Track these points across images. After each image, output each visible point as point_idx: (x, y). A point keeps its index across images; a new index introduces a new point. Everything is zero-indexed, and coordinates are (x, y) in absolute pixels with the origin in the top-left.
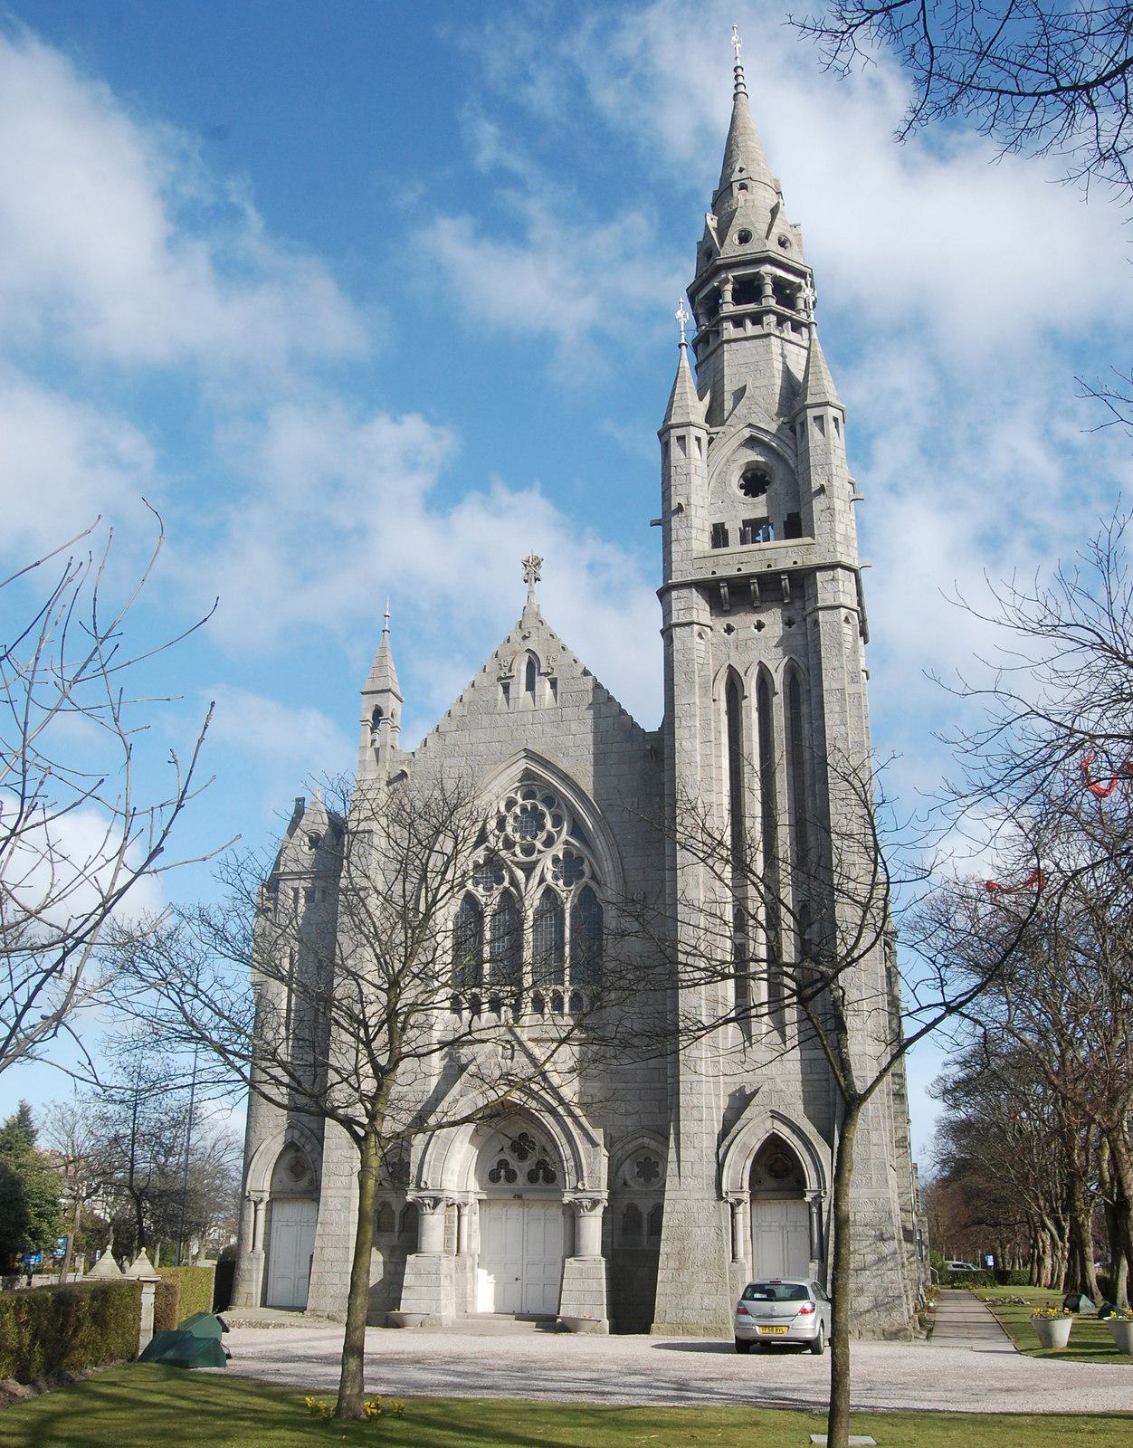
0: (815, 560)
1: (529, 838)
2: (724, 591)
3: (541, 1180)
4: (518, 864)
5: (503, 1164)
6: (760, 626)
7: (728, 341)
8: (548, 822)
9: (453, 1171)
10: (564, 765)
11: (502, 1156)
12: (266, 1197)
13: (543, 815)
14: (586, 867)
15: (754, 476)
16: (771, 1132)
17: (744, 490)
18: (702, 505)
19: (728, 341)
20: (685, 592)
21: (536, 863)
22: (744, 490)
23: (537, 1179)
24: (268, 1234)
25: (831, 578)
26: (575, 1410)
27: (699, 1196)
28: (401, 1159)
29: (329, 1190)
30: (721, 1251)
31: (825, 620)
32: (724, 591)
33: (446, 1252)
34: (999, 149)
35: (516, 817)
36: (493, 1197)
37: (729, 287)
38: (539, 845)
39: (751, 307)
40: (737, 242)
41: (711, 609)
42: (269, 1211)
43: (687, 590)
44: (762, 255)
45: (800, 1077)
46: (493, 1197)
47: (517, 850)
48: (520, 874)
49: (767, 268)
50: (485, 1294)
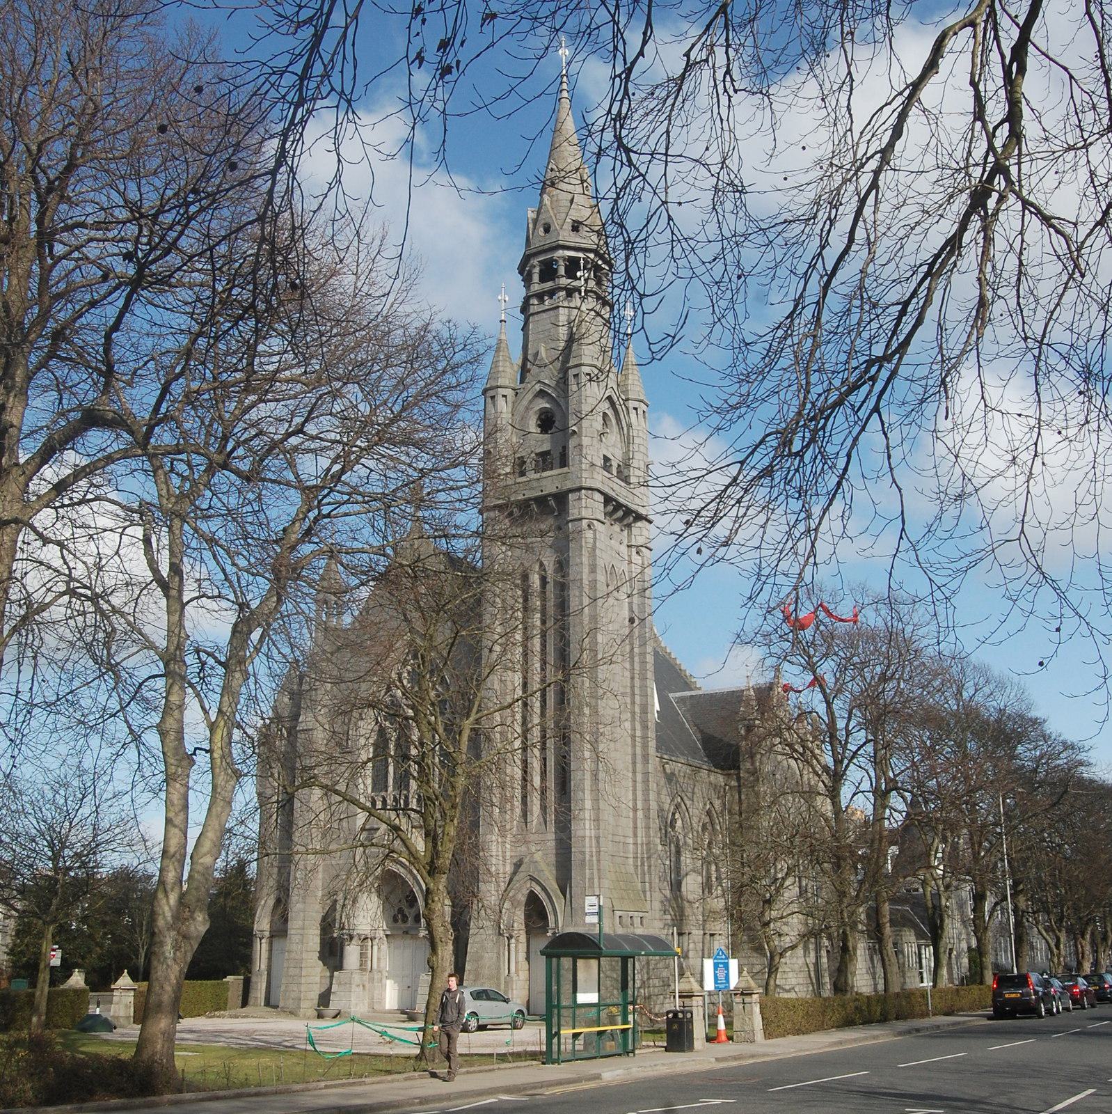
0: (569, 485)
5: (400, 911)
7: (533, 314)
12: (267, 934)
15: (547, 416)
19: (533, 314)
24: (270, 959)
26: (1018, 1033)
28: (1028, 779)
33: (361, 970)
34: (885, 63)
36: (395, 933)
37: (537, 270)
39: (549, 284)
40: (543, 234)
42: (271, 944)
44: (553, 245)
45: (554, 851)
46: (395, 933)
49: (561, 253)
50: (391, 996)
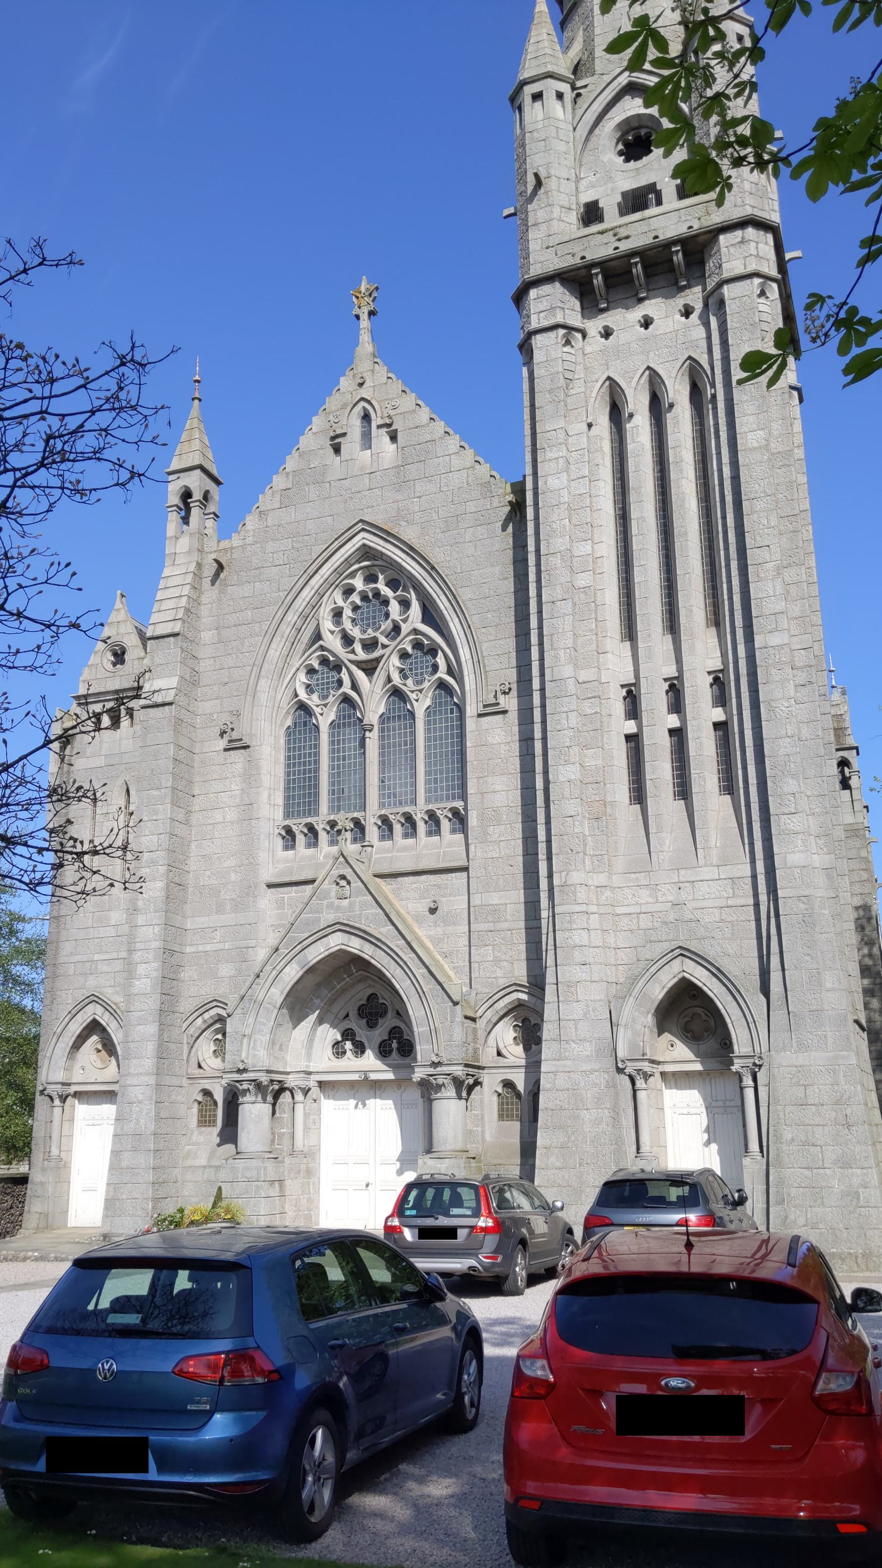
1: (370, 631)
2: (598, 281)
3: (349, 1053)
4: (359, 664)
6: (647, 323)
8: (394, 608)
9: (281, 1045)
10: (409, 534)
11: (347, 1025)
13: (386, 602)
14: (440, 660)
16: (680, 976)
17: (623, 157)
18: (566, 176)
20: (546, 289)
21: (378, 660)
22: (623, 157)
23: (391, 1051)
25: (739, 239)
27: (586, 1067)
29: (129, 1078)
30: (618, 1142)
31: (732, 295)
32: (598, 281)
35: (356, 608)
38: (383, 640)
41: (582, 308)
43: (549, 286)
47: (358, 647)
48: (360, 675)
